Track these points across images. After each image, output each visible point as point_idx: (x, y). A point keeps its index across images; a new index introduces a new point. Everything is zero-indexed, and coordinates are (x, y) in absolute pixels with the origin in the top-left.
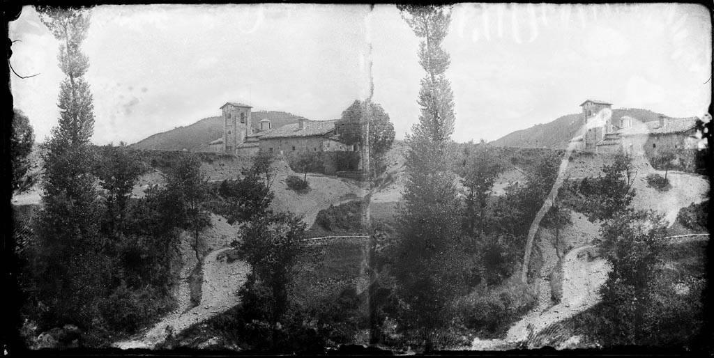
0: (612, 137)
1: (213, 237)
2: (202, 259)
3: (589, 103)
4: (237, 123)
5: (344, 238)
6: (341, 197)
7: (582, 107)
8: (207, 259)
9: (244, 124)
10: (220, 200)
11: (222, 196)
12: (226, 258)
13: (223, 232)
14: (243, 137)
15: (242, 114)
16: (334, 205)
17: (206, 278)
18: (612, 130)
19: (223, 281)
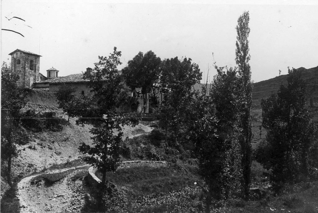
0: (40, 86)
1: (19, 166)
2: (15, 185)
3: (19, 53)
4: (27, 69)
5: (133, 162)
6: (133, 132)
7: (10, 56)
8: (20, 185)
9: (33, 71)
10: (23, 131)
11: (25, 127)
12: (43, 182)
13: (29, 161)
14: (32, 83)
15: (32, 61)
16: (129, 138)
17: (22, 203)
18: (40, 80)
19: (44, 205)
